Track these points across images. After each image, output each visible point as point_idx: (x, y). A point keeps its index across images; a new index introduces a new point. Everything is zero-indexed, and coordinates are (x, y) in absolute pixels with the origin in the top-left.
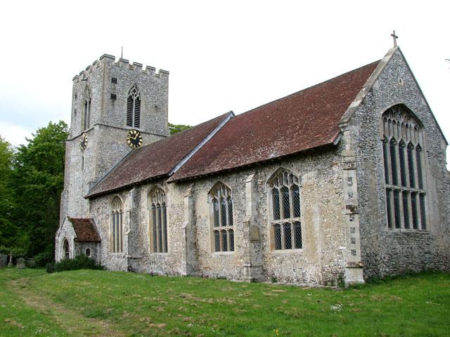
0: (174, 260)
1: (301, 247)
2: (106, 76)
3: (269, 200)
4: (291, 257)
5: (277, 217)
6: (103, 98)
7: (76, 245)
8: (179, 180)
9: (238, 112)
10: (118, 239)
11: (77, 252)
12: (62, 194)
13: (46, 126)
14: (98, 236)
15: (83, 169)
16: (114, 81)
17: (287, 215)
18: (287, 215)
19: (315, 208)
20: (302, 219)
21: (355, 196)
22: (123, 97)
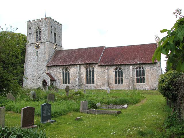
0: (74, 85)
3: (135, 72)
4: (142, 85)
5: (137, 76)
9: (107, 46)
16: (51, 27)
17: (119, 77)
18: (140, 75)
19: (149, 75)
20: (145, 77)
21: (161, 73)
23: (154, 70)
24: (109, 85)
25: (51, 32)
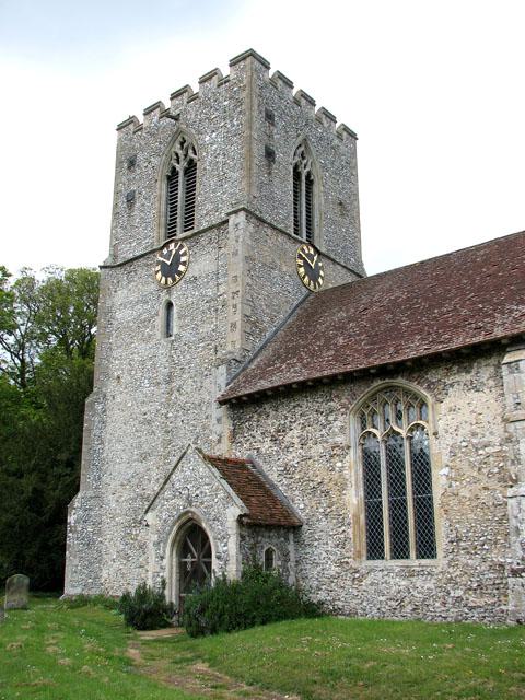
1: (434, 556)
2: (256, 101)
6: (250, 150)
7: (242, 537)
8: (239, 398)
10: (398, 507)
11: (246, 558)
12: (87, 401)
13: (342, 119)
14: (287, 513)
15: (168, 334)
22: (286, 158)
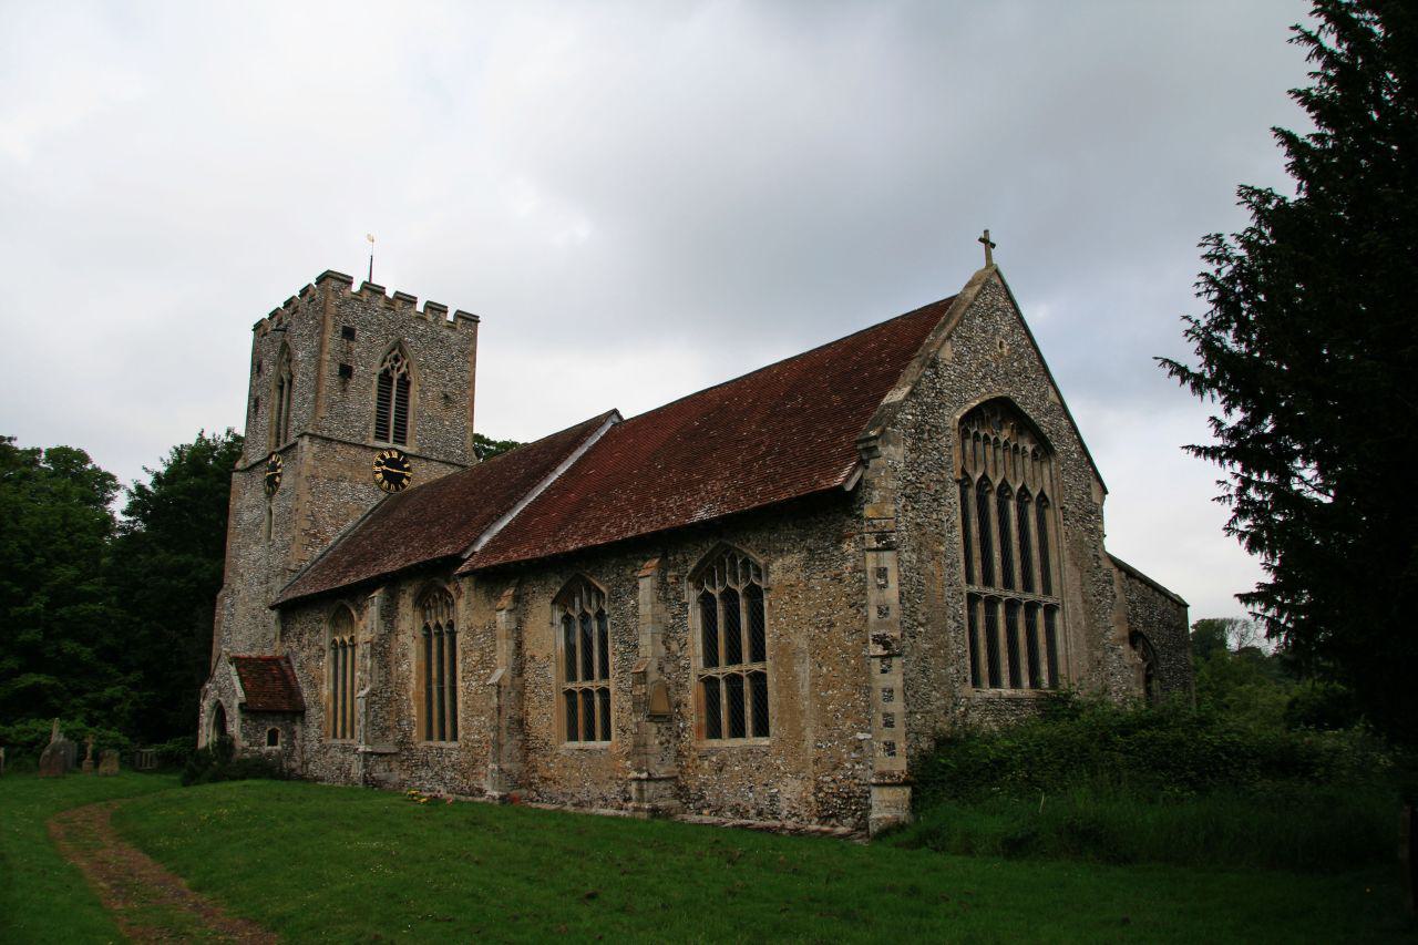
16: (349, 334)
20: (769, 666)
23: (838, 578)
24: (531, 756)
25: (346, 372)
